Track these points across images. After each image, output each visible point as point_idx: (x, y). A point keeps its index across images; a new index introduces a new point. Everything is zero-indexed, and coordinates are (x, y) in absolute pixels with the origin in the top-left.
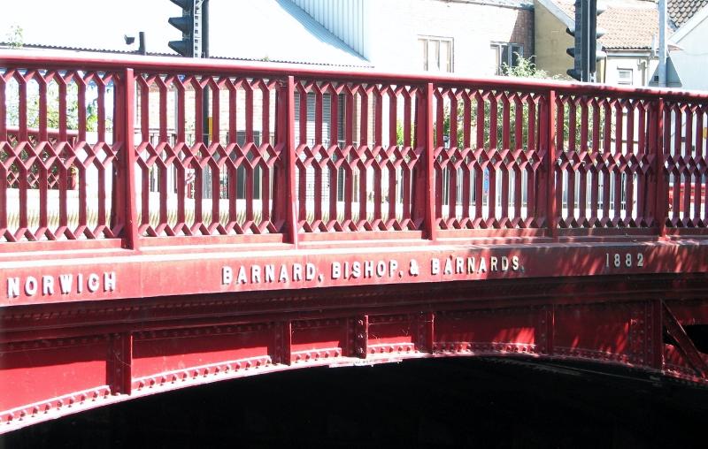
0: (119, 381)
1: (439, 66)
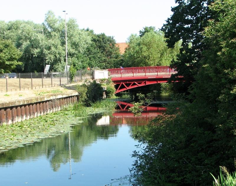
0: (157, 82)
1: (63, 11)
